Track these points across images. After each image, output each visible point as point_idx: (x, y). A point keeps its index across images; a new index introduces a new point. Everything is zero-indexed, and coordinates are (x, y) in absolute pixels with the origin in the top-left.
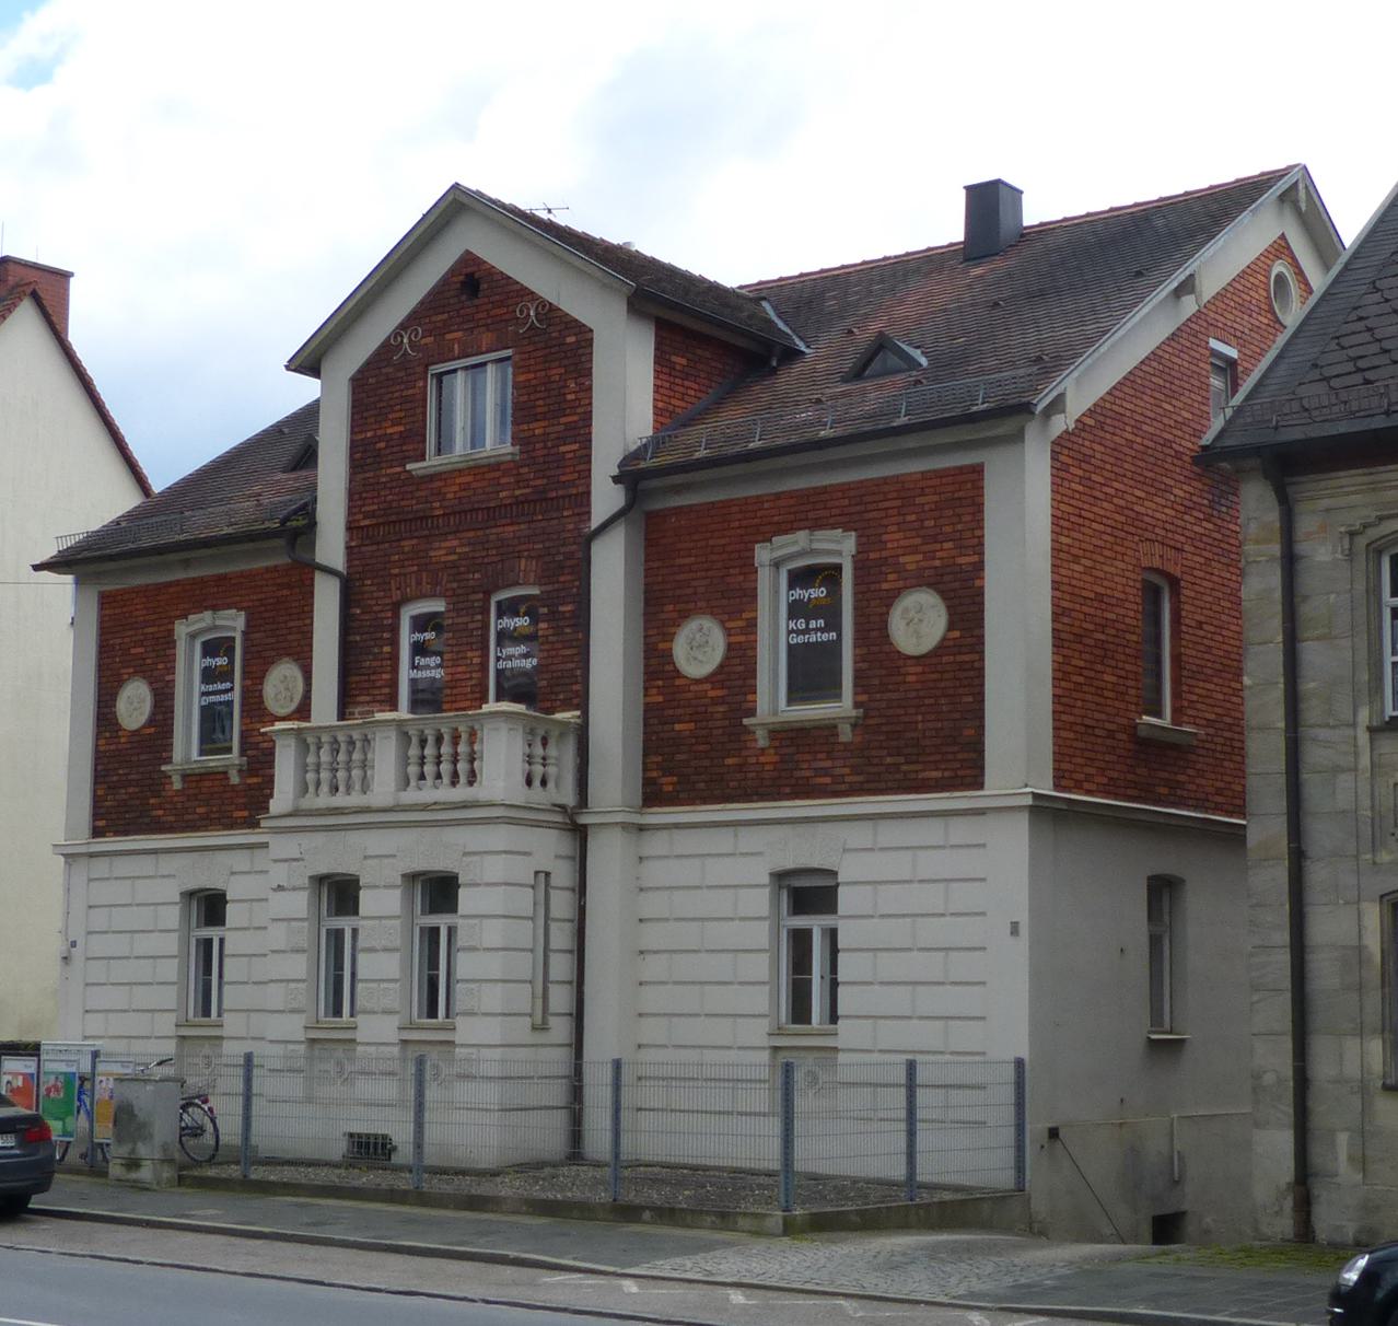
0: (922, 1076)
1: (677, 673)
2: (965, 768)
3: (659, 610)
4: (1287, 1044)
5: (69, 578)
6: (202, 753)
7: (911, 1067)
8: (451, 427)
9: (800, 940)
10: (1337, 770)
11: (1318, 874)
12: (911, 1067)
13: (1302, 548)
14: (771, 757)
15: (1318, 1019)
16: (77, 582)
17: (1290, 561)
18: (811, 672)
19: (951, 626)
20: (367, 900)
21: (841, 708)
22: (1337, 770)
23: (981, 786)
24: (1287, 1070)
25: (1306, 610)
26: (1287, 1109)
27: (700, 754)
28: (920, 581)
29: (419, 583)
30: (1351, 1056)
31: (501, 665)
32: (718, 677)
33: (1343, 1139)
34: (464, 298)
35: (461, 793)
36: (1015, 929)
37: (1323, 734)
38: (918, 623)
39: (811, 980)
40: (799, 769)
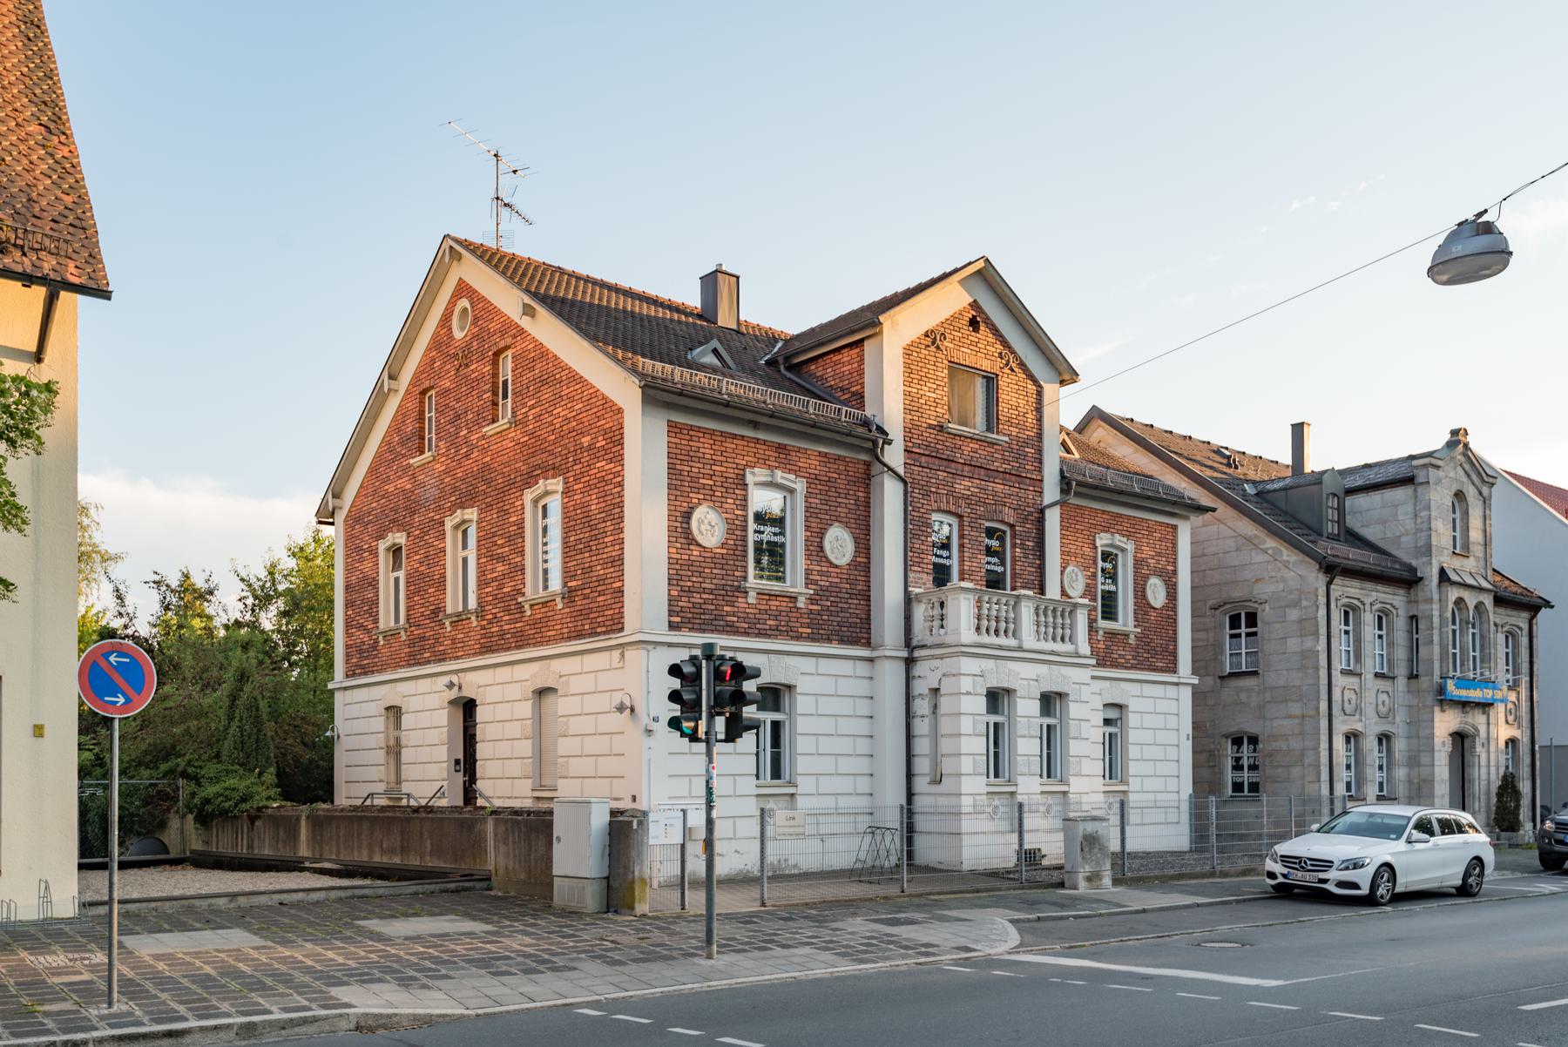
2: (1172, 669)
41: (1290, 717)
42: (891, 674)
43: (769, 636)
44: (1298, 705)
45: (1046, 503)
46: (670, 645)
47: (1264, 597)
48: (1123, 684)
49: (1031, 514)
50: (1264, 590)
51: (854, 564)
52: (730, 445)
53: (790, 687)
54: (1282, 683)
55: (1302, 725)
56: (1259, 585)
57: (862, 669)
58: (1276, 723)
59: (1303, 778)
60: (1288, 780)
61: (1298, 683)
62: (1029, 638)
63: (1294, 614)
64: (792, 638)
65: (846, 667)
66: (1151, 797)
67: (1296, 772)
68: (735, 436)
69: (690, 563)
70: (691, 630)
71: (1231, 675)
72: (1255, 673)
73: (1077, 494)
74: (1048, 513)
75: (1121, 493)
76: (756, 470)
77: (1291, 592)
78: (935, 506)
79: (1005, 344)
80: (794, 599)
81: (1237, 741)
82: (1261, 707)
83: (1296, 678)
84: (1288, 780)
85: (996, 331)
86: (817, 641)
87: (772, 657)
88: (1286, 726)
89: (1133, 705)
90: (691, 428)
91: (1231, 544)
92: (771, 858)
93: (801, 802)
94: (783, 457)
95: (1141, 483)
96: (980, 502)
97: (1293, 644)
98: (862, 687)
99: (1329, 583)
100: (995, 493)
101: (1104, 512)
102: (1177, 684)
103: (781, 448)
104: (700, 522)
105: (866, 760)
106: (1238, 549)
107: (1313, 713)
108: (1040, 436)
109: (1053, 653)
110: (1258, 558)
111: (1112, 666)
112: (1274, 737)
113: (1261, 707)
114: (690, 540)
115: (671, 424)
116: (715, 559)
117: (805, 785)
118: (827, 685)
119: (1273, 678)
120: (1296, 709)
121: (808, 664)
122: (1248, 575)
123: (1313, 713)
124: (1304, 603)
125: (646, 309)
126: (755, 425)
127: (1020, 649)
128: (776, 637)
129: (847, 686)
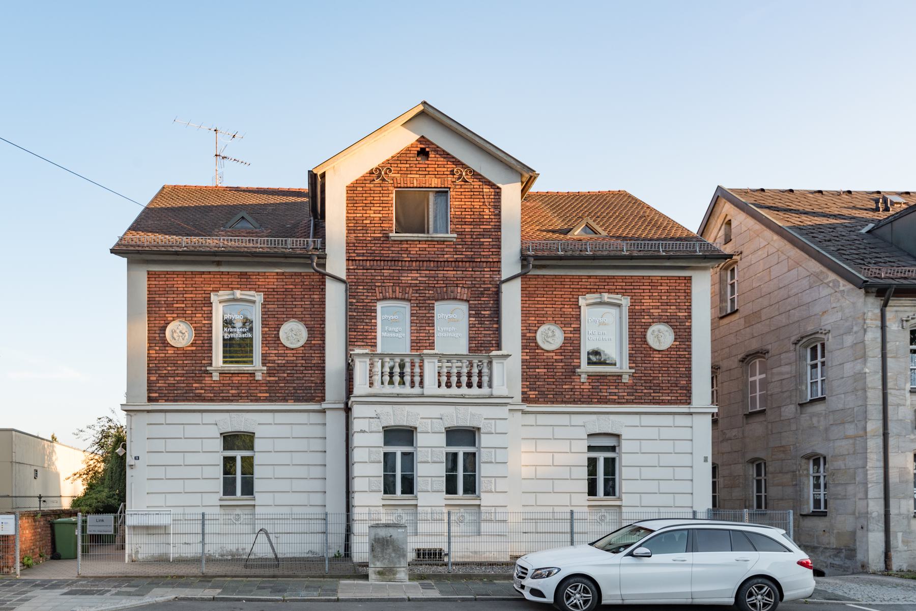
0: (206, 517)
1: (538, 347)
2: (685, 397)
3: (531, 320)
4: (882, 502)
5: (125, 260)
6: (224, 362)
7: (572, 513)
8: (712, 226)
9: (229, 462)
10: (898, 405)
11: (892, 442)
12: (572, 513)
13: (888, 323)
14: (587, 386)
15: (892, 493)
16: (130, 263)
17: (883, 327)
18: (237, 349)
19: (675, 340)
20: (421, 439)
21: (257, 365)
22: (898, 405)
23: (689, 403)
24: (882, 512)
25: (889, 346)
26: (882, 525)
27: (553, 382)
28: (660, 320)
29: (394, 292)
30: (902, 507)
31: (385, 334)
32: (561, 350)
33: (900, 535)
34: (419, 159)
35: (417, 390)
36: (706, 460)
37: (893, 392)
38: (293, 334)
39: (605, 475)
40: (603, 390)
41: (846, 438)
42: (335, 420)
43: (232, 401)
44: (853, 426)
45: (504, 277)
46: (148, 411)
47: (828, 328)
48: (612, 417)
49: (488, 289)
50: (829, 321)
51: (308, 345)
52: (198, 279)
53: (479, 429)
54: (840, 406)
55: (854, 444)
56: (825, 317)
57: (315, 418)
58: (838, 443)
59: (855, 495)
60: (845, 497)
61: (851, 405)
62: (431, 385)
63: (849, 340)
64: (252, 401)
65: (303, 418)
66: (286, 510)
67: (850, 488)
68: (203, 273)
69: (166, 360)
70: (166, 401)
71: (812, 401)
72: (824, 398)
73: (535, 267)
74: (504, 287)
75: (572, 258)
76: (221, 292)
77: (846, 320)
78: (380, 296)
79: (457, 163)
80: (252, 374)
81: (816, 462)
82: (827, 430)
83: (851, 401)
84: (845, 497)
85: (446, 155)
86: (275, 401)
87: (233, 415)
88: (843, 446)
89: (625, 433)
90: (167, 273)
91: (805, 283)
92: (206, 552)
93: (258, 510)
94: (245, 282)
95: (611, 246)
96: (428, 287)
97: (849, 369)
98: (317, 431)
99: (885, 305)
100: (446, 278)
101: (590, 277)
102: (691, 414)
103: (242, 275)
104: (173, 332)
105: (319, 482)
106: (810, 287)
107: (861, 433)
108: (498, 228)
109: (398, 396)
110: (825, 292)
111: (599, 402)
112: (835, 457)
113: (827, 430)
114: (165, 344)
115: (148, 272)
116: (182, 353)
117: (626, 500)
118: (285, 431)
119: (835, 402)
120: (850, 430)
121: (267, 417)
122: (817, 309)
123: (861, 433)
124: (855, 329)
125: (273, 200)
126: (219, 263)
127: (422, 396)
128: (237, 401)
129: (299, 431)
